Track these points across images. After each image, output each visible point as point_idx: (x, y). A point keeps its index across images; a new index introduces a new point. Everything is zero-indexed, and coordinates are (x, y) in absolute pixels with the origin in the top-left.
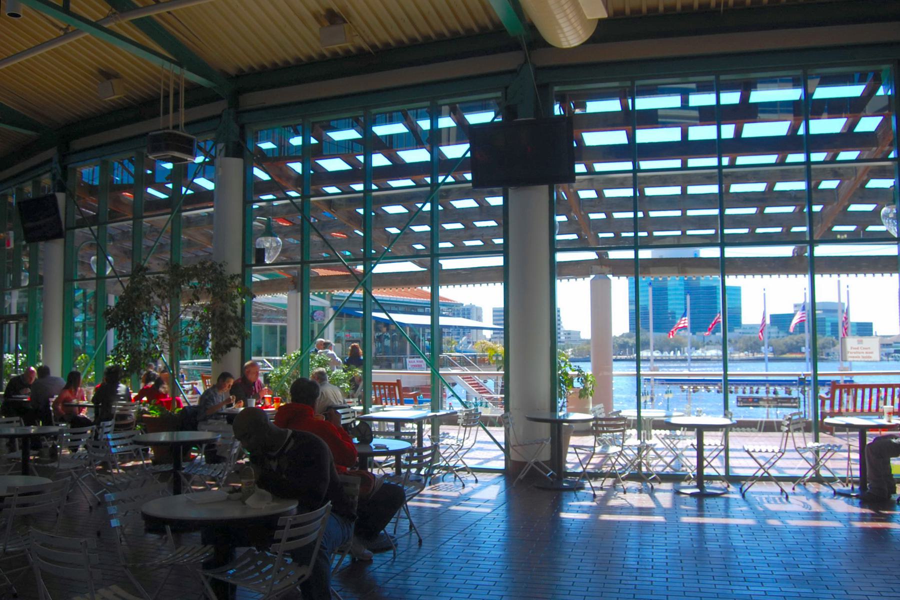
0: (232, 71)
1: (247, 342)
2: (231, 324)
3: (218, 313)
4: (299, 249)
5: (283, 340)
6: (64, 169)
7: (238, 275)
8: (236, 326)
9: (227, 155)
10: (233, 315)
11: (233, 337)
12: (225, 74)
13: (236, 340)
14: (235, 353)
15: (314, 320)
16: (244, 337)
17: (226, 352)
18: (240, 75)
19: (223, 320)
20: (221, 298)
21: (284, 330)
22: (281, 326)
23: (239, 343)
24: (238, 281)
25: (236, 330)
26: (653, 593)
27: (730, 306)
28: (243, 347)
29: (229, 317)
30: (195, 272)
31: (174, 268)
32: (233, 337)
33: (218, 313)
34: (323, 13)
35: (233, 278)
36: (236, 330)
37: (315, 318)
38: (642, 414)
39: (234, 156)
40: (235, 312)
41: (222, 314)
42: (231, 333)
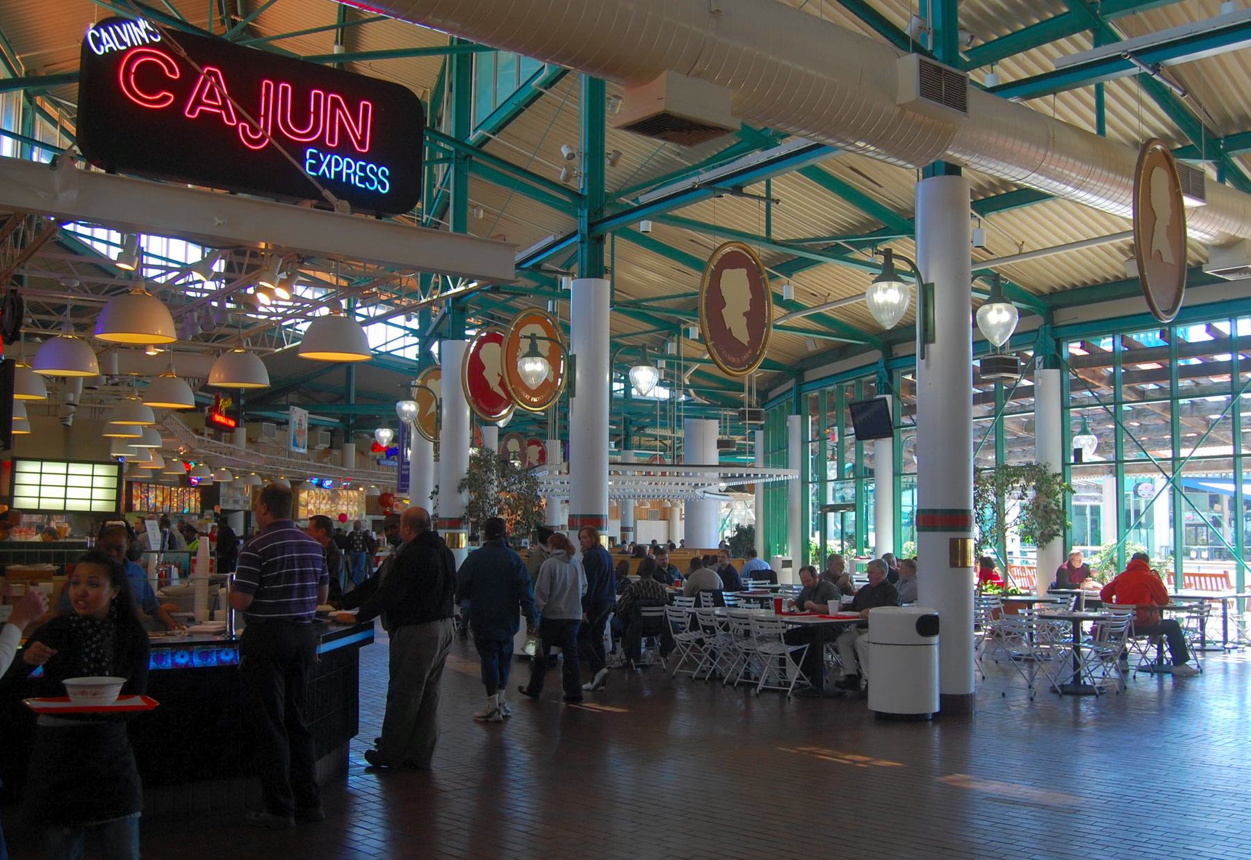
0: (1046, 290)
1: (1068, 532)
2: (1054, 516)
3: (1041, 507)
4: (1113, 434)
5: (1095, 523)
6: (890, 373)
7: (1060, 474)
8: (1058, 518)
9: (1045, 367)
10: (124, 48)
11: (1056, 527)
12: (1041, 295)
13: (1058, 530)
14: (1058, 541)
15: (1140, 496)
16: (1065, 528)
17: (1050, 541)
18: (1054, 292)
19: (1046, 512)
20: (1046, 494)
21: (1096, 511)
22: (1092, 507)
23: (1061, 533)
24: (1059, 479)
25: (1059, 521)
26: (1220, 605)
27: (1188, 522)
28: (1065, 536)
29: (1052, 510)
30: (1018, 472)
31: (1001, 468)
32: (1056, 527)
33: (1041, 507)
34: (1127, 248)
35: (1055, 476)
36: (1059, 521)
37: (1140, 494)
38: (833, 478)
39: (1051, 368)
40: (1058, 506)
41: (1045, 507)
42: (1054, 524)
